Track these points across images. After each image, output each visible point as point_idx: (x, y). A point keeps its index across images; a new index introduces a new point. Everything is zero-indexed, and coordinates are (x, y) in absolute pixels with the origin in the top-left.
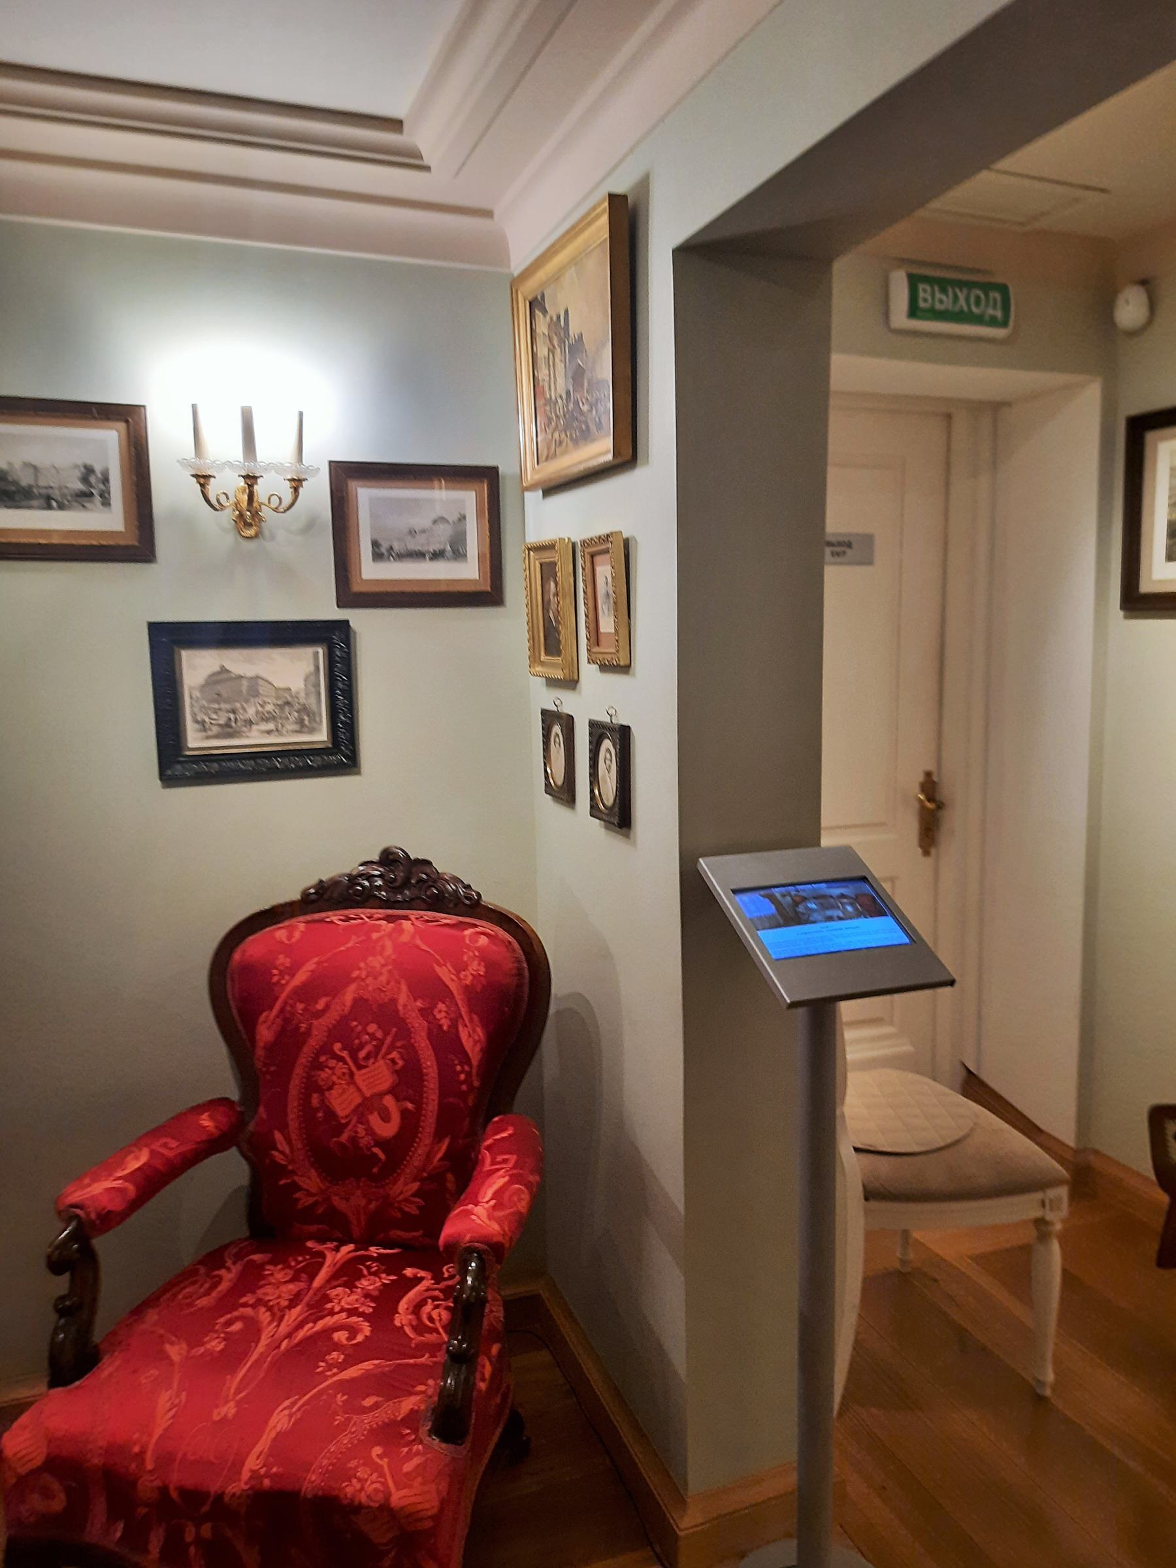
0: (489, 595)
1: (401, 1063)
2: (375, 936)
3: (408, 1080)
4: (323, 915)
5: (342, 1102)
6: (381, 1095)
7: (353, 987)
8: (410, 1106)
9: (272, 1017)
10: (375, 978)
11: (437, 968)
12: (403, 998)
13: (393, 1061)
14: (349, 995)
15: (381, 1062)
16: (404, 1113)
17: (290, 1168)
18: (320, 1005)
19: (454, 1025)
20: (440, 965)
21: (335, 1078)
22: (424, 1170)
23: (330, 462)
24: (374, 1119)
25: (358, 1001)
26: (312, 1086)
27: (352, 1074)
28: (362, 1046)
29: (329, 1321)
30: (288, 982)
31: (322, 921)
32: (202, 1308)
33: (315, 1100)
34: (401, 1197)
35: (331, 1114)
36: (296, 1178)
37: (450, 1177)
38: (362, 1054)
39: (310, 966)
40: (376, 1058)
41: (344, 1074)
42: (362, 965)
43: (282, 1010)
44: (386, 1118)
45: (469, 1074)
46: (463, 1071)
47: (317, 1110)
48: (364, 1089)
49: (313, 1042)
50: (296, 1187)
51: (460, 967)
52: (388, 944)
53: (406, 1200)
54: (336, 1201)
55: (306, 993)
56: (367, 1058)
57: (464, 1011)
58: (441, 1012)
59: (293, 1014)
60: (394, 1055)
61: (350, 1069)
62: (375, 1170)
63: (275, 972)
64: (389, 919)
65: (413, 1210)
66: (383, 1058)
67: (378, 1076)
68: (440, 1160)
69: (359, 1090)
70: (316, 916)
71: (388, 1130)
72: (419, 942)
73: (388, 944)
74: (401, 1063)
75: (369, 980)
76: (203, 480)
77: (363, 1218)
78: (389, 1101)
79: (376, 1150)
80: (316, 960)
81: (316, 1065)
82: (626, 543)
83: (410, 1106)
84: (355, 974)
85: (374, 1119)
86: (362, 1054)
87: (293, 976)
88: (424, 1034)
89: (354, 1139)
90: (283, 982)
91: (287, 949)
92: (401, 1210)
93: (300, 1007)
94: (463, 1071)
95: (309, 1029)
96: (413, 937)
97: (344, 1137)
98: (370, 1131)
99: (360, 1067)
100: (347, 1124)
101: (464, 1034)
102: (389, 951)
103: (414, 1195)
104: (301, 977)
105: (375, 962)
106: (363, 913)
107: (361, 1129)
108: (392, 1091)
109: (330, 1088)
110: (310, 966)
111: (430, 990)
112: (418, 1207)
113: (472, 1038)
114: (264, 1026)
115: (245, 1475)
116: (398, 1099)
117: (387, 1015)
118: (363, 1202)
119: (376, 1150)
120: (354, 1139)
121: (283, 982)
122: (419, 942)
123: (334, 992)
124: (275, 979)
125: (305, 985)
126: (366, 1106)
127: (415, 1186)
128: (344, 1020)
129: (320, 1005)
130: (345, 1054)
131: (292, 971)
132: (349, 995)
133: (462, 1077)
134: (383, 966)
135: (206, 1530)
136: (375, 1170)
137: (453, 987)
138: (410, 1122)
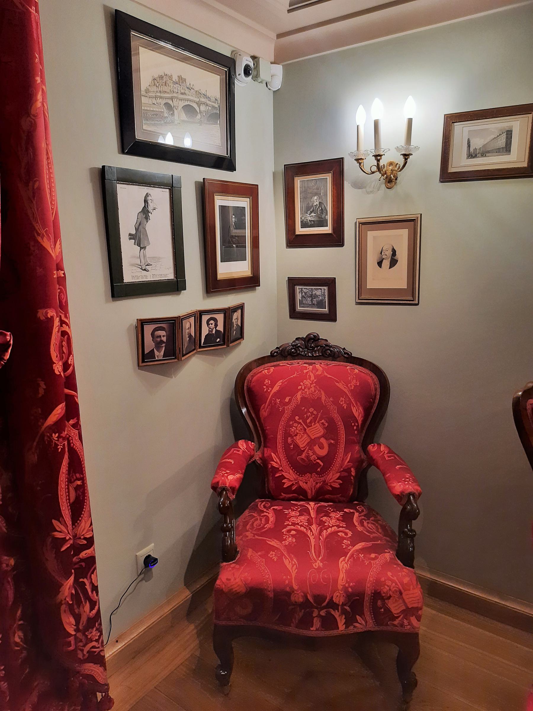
0: (366, 225)
1: (327, 424)
2: (305, 371)
3: (331, 431)
4: (278, 363)
5: (302, 441)
6: (319, 438)
7: (300, 393)
8: (332, 442)
9: (266, 406)
10: (309, 389)
11: (337, 384)
12: (323, 398)
13: (322, 423)
14: (299, 395)
15: (317, 424)
16: (330, 445)
17: (280, 469)
18: (287, 400)
19: (349, 407)
20: (338, 382)
21: (297, 431)
22: (341, 467)
23: (342, 158)
24: (316, 448)
25: (303, 398)
26: (287, 434)
27: (305, 430)
28: (308, 418)
29: (329, 530)
30: (271, 391)
31: (278, 365)
32: (270, 528)
33: (289, 440)
34: (331, 481)
35: (296, 446)
36: (283, 473)
37: (352, 469)
38: (308, 421)
39: (279, 383)
40: (315, 423)
41: (301, 429)
42: (302, 384)
43: (270, 402)
44: (321, 447)
45: (358, 426)
46: (355, 425)
47: (291, 444)
48: (311, 436)
49: (286, 415)
50: (283, 477)
51: (347, 383)
52: (312, 375)
53: (334, 482)
54: (301, 483)
55: (280, 394)
56: (311, 422)
57: (352, 400)
58: (342, 401)
59: (275, 404)
60: (323, 421)
61: (304, 427)
62: (319, 469)
63: (265, 387)
64: (310, 364)
65: (337, 486)
66: (318, 422)
67: (317, 430)
68: (348, 462)
69: (309, 436)
70: (275, 363)
71: (323, 452)
72: (326, 374)
73: (312, 375)
74: (327, 424)
75: (306, 390)
76: (378, 157)
77: (314, 491)
78: (323, 440)
79: (318, 461)
80: (281, 381)
81: (288, 426)
82: (280, 36)
83: (332, 442)
84: (299, 387)
85: (316, 448)
86: (308, 421)
87: (272, 388)
88: (336, 411)
89: (308, 457)
90: (269, 391)
91: (266, 377)
92: (331, 486)
93: (278, 401)
94: (355, 425)
95: (283, 411)
96: (323, 372)
97: (303, 456)
98: (314, 453)
99: (308, 427)
100: (304, 451)
101: (354, 411)
102: (313, 378)
103: (337, 479)
104: (276, 388)
105: (307, 382)
106: (301, 362)
107: (311, 453)
108: (323, 436)
109: (296, 435)
110: (279, 383)
111: (335, 394)
112: (339, 484)
113: (358, 412)
114: (263, 410)
115: (340, 587)
116: (326, 439)
117: (316, 403)
118: (314, 483)
119: (318, 461)
120: (308, 457)
121: (269, 391)
122: (326, 374)
123: (292, 394)
124: (265, 390)
125: (279, 391)
126: (312, 442)
127: (338, 474)
128: (298, 407)
129: (287, 400)
130: (301, 421)
131: (272, 386)
132: (299, 395)
133: (355, 428)
134: (311, 384)
135: (323, 613)
136: (319, 469)
137: (346, 390)
138: (333, 448)
